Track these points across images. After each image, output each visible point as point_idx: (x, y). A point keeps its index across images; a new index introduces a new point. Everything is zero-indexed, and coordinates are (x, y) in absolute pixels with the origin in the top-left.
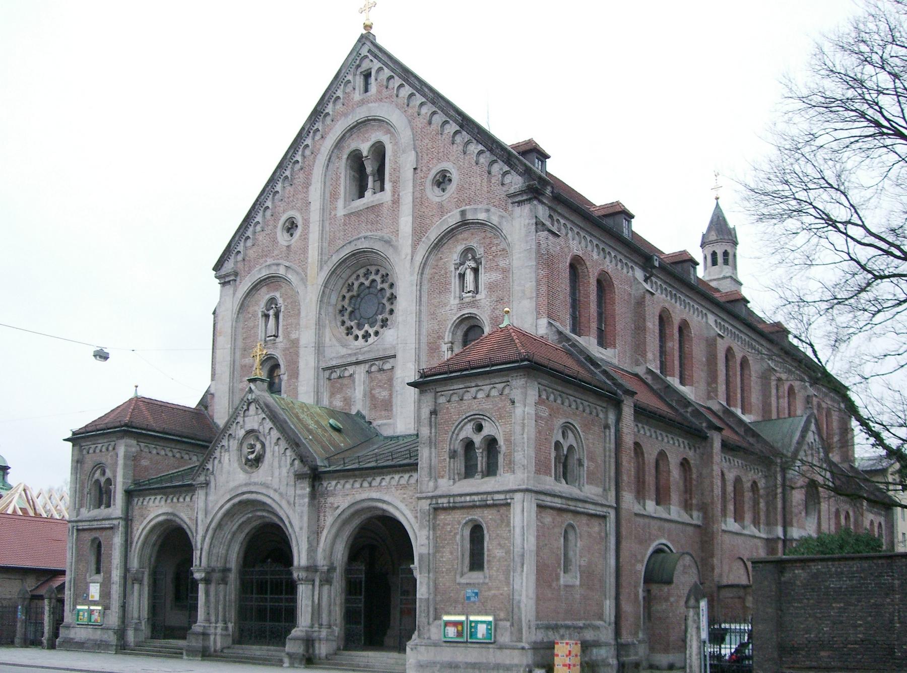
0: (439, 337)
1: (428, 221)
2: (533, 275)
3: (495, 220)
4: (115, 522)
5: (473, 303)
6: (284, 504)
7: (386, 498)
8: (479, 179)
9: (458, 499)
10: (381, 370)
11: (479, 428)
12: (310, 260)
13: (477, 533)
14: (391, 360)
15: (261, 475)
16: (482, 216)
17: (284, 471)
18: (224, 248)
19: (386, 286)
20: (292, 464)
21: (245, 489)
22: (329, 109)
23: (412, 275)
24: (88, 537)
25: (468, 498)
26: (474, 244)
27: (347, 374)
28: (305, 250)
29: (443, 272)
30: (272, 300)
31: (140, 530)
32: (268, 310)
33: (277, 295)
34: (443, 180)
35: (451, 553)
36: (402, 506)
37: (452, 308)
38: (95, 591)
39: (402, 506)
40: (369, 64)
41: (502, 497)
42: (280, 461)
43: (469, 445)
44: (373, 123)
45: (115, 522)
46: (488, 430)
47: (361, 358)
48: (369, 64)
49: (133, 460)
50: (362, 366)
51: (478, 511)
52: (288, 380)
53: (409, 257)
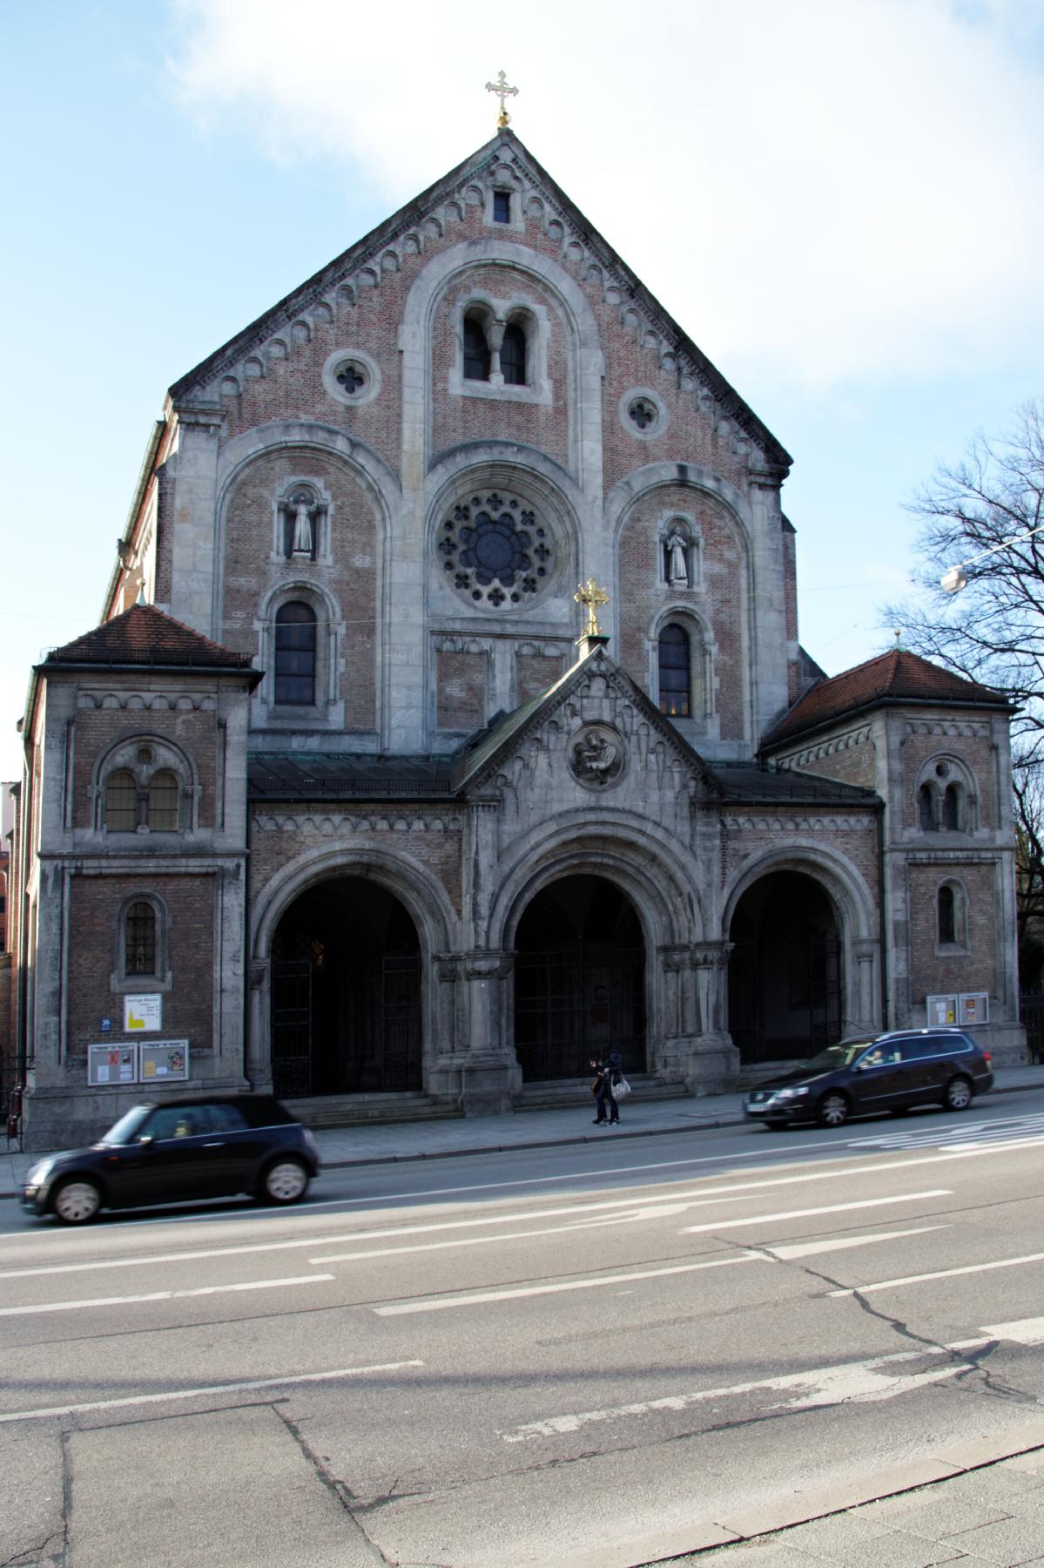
0: (639, 629)
1: (624, 461)
2: (781, 583)
3: (728, 494)
4: (230, 864)
5: (689, 595)
6: (674, 845)
7: (822, 847)
8: (699, 433)
9: (940, 854)
10: (539, 655)
11: (145, 755)
12: (406, 446)
13: (946, 895)
14: (562, 645)
15: (621, 796)
16: (710, 484)
17: (670, 795)
18: (201, 360)
19: (486, 591)
20: (685, 786)
21: (591, 817)
22: (441, 213)
23: (605, 528)
24: (933, 879)
25: (952, 854)
26: (690, 516)
27: (474, 648)
28: (393, 422)
29: (642, 539)
30: (303, 493)
31: (281, 884)
32: (297, 502)
33: (319, 483)
34: (642, 413)
35: (927, 921)
36: (844, 859)
37: (658, 600)
38: (143, 1011)
39: (844, 859)
40: (503, 179)
41: (989, 855)
42: (660, 779)
43: (926, 789)
44: (515, 275)
45: (230, 864)
46: (954, 774)
47: (510, 629)
48: (503, 179)
49: (906, 752)
50: (508, 642)
51: (957, 870)
52: (348, 635)
53: (599, 502)
